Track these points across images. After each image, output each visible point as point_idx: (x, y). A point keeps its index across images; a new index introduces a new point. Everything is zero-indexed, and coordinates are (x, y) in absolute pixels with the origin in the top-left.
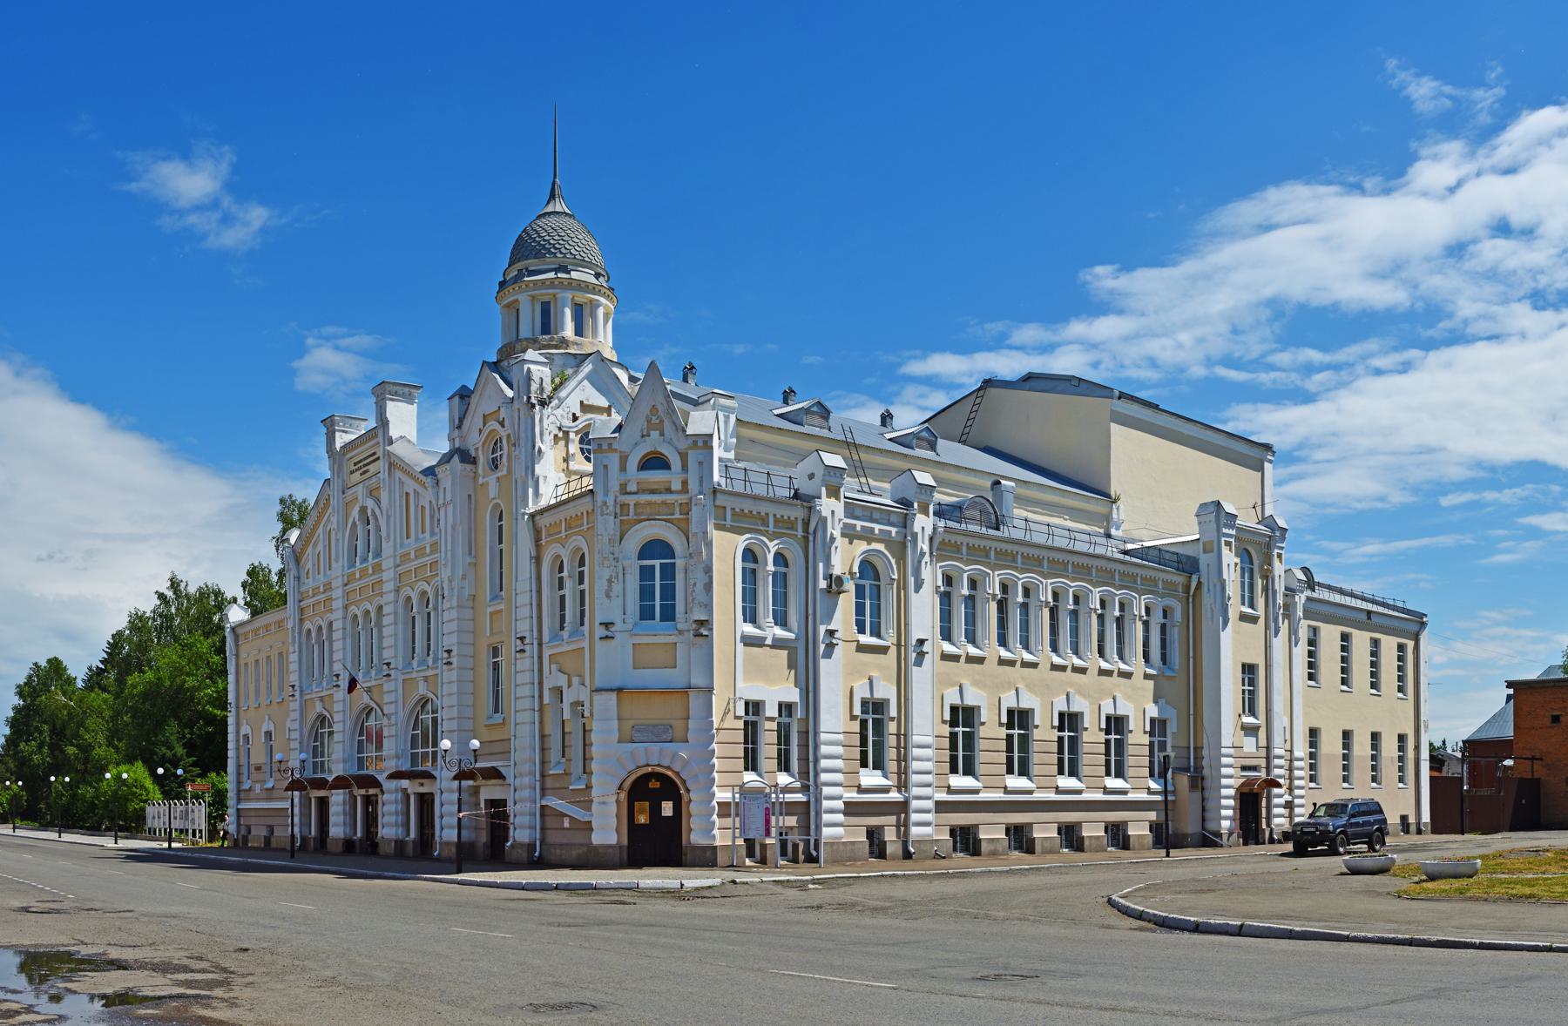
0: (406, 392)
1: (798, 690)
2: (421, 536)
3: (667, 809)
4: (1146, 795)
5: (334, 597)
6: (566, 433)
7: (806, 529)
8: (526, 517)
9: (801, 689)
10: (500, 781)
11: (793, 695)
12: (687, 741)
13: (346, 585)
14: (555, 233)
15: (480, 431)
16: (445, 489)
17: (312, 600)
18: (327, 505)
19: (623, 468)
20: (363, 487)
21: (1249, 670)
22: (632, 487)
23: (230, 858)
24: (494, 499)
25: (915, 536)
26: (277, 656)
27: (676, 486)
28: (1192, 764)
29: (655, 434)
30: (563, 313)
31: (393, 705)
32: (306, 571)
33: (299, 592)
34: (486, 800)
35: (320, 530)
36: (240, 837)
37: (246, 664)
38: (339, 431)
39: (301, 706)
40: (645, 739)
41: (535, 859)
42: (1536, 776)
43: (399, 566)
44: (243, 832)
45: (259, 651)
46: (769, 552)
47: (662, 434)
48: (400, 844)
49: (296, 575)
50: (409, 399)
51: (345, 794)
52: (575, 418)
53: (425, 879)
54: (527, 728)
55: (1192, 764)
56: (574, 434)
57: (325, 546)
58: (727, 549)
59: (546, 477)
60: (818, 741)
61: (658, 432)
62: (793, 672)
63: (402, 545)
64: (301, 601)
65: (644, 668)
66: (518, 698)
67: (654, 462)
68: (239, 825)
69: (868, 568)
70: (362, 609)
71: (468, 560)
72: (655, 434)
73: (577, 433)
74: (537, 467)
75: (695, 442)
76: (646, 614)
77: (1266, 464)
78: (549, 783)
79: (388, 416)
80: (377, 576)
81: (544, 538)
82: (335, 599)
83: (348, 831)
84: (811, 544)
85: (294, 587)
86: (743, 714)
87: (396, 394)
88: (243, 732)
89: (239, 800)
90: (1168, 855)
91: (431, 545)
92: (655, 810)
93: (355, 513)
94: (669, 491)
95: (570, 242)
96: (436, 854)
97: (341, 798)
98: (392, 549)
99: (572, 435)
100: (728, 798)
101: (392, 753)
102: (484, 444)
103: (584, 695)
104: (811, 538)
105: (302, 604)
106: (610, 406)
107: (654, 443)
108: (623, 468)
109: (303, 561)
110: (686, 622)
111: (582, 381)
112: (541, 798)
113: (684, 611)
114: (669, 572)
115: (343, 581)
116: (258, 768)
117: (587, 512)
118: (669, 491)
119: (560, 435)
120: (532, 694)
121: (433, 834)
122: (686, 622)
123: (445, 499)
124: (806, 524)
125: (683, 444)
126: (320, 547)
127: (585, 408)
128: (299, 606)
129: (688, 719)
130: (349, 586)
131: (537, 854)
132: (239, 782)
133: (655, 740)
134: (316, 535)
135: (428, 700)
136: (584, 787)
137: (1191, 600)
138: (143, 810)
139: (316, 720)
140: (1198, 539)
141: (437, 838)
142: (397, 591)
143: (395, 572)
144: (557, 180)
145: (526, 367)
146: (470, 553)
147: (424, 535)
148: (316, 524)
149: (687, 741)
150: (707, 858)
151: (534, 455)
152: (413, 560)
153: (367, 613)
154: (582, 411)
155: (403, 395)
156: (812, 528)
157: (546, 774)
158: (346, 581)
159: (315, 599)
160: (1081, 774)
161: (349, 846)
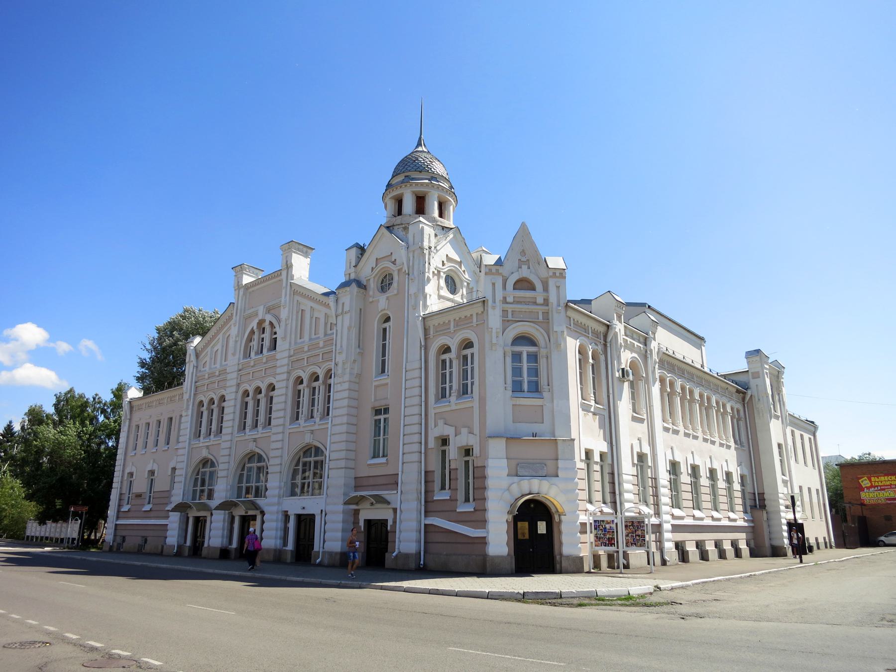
0: (306, 250)
1: (606, 443)
2: (329, 332)
3: (542, 527)
4: (692, 521)
5: (228, 378)
6: (439, 272)
7: (605, 340)
8: (421, 318)
9: (608, 443)
10: (385, 506)
11: (604, 447)
12: (558, 476)
13: (240, 370)
14: (427, 160)
15: (373, 269)
16: (343, 304)
17: (207, 381)
18: (230, 318)
19: (504, 287)
20: (264, 307)
21: (780, 446)
22: (510, 299)
23: (162, 565)
24: (384, 310)
25: (651, 351)
26: (144, 425)
27: (540, 300)
28: (758, 503)
29: (525, 267)
30: (434, 204)
31: (280, 450)
32: (204, 362)
33: (196, 376)
34: (365, 520)
35: (220, 336)
36: (115, 544)
37: (138, 426)
38: (245, 274)
39: (188, 452)
40: (526, 474)
41: (422, 566)
42: (864, 515)
43: (291, 356)
44: (119, 540)
45: (140, 419)
46: (590, 350)
47: (529, 268)
48: (111, 547)
49: (195, 365)
50: (306, 255)
51: (225, 514)
52: (443, 264)
53: (382, 588)
54: (415, 466)
55: (758, 503)
56: (443, 273)
57: (223, 346)
58: (572, 345)
59: (430, 295)
60: (621, 480)
61: (527, 266)
62: (602, 431)
63: (296, 343)
64: (196, 382)
65: (520, 422)
66: (405, 444)
67: (524, 284)
68: (115, 535)
69: (633, 364)
70: (254, 386)
71: (358, 350)
72: (525, 267)
73: (444, 273)
74: (426, 287)
75: (554, 274)
76: (517, 388)
77: (703, 347)
78: (121, 515)
79: (292, 262)
80: (330, 348)
81: (431, 333)
82: (229, 380)
83: (225, 542)
84: (609, 349)
85: (193, 373)
86: (599, 461)
87: (298, 250)
88: (127, 471)
89: (118, 518)
90: (801, 562)
91: (294, 350)
92: (533, 528)
93: (254, 324)
94: (535, 303)
95: (436, 166)
96: (318, 561)
97: (222, 517)
98: (288, 344)
99: (442, 274)
100: (586, 520)
101: (222, 490)
102: (374, 277)
103: (473, 441)
104: (608, 345)
105: (197, 384)
106: (461, 261)
107: (525, 273)
108: (504, 287)
109: (201, 356)
110: (549, 391)
111: (447, 243)
112: (116, 521)
113: (547, 384)
114: (533, 358)
115: (289, 353)
116: (139, 496)
117: (477, 314)
118: (535, 303)
119: (436, 272)
120: (420, 441)
121: (203, 542)
122: (549, 391)
123: (190, 359)
124: (605, 336)
125: (544, 274)
126: (219, 347)
127: (449, 259)
128: (195, 385)
129: (557, 459)
130: (242, 372)
131: (422, 562)
132: (120, 506)
133: (535, 474)
134: (218, 338)
135: (208, 461)
136: (473, 510)
137: (746, 405)
138: (652, 525)
139: (301, 450)
140: (748, 371)
141: (206, 545)
142: (238, 385)
143: (289, 360)
144: (422, 136)
145: (421, 225)
146: (359, 346)
147: (332, 332)
148: (217, 332)
149: (558, 476)
150: (576, 567)
151: (424, 282)
152: (306, 352)
153: (212, 401)
154: (447, 261)
155: (302, 252)
156: (609, 339)
157: (429, 500)
158: (292, 353)
159: (209, 380)
160: (681, 507)
161: (224, 554)
